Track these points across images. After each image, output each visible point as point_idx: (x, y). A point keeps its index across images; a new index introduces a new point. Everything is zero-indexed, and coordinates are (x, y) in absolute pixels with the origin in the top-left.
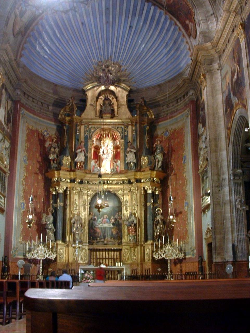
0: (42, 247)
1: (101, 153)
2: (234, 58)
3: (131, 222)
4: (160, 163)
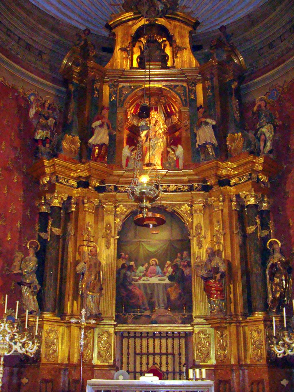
0: (7, 325)
3: (214, 268)
4: (269, 144)
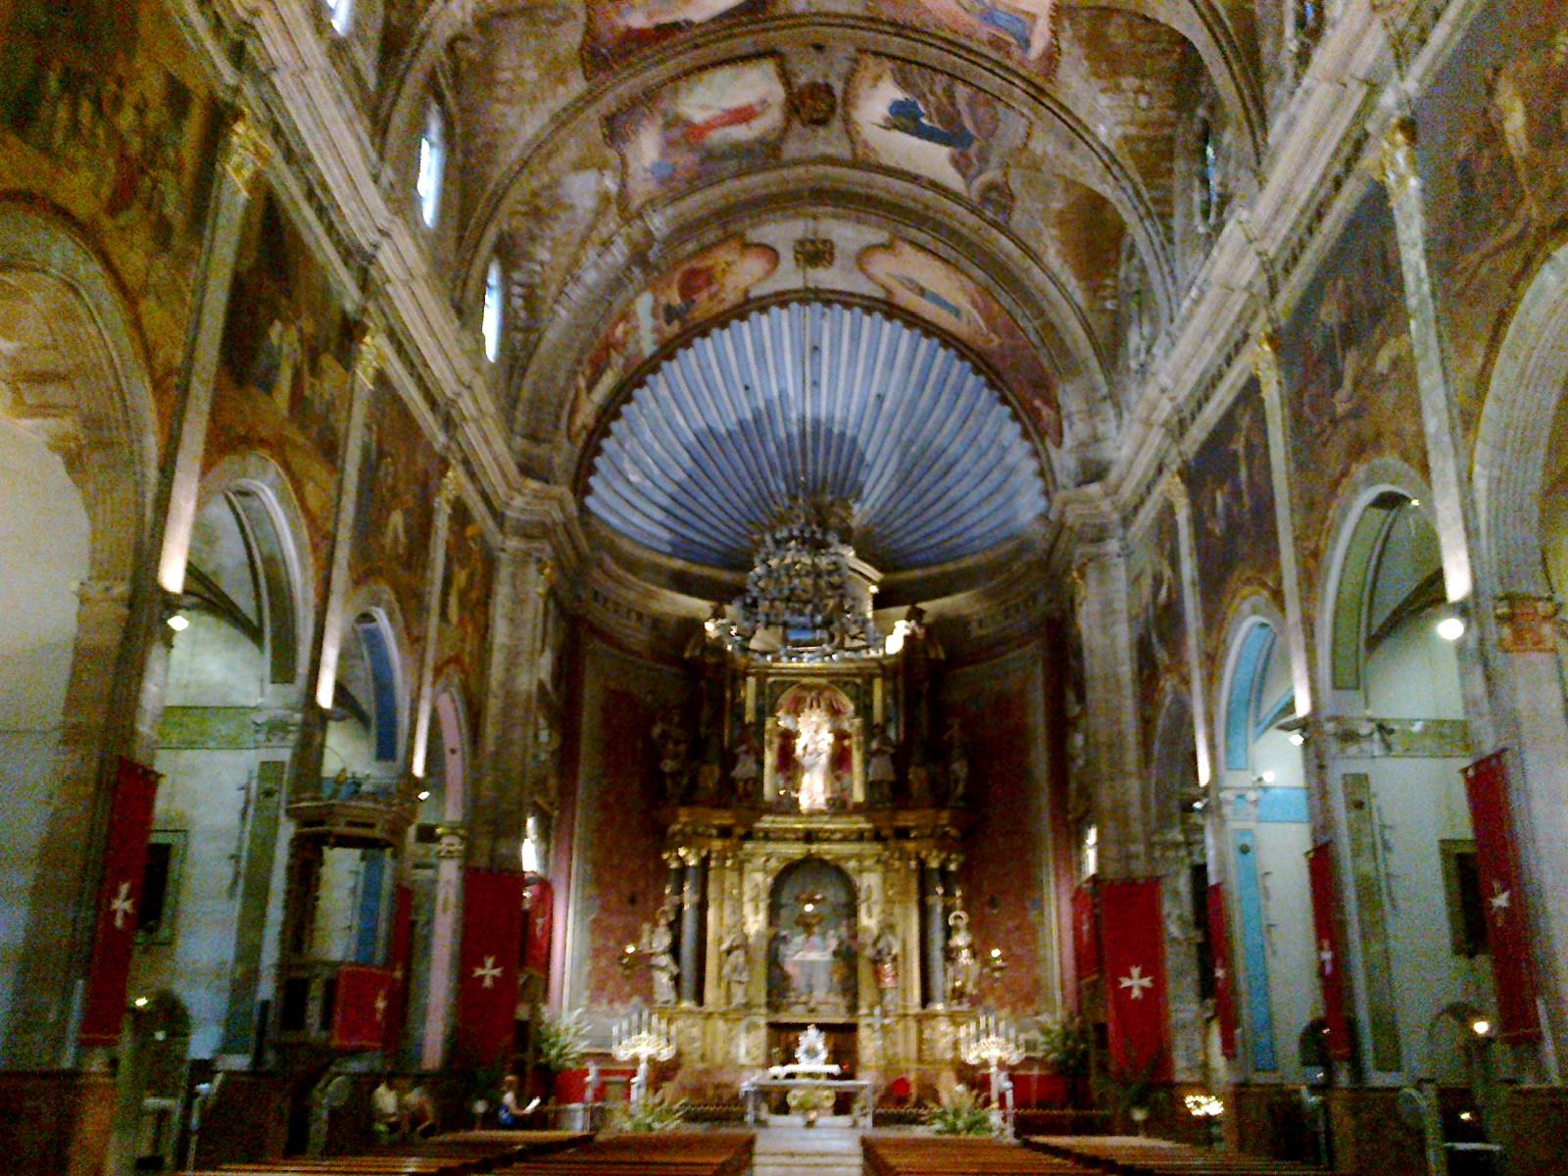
1: (799, 751)
2: (1162, 547)
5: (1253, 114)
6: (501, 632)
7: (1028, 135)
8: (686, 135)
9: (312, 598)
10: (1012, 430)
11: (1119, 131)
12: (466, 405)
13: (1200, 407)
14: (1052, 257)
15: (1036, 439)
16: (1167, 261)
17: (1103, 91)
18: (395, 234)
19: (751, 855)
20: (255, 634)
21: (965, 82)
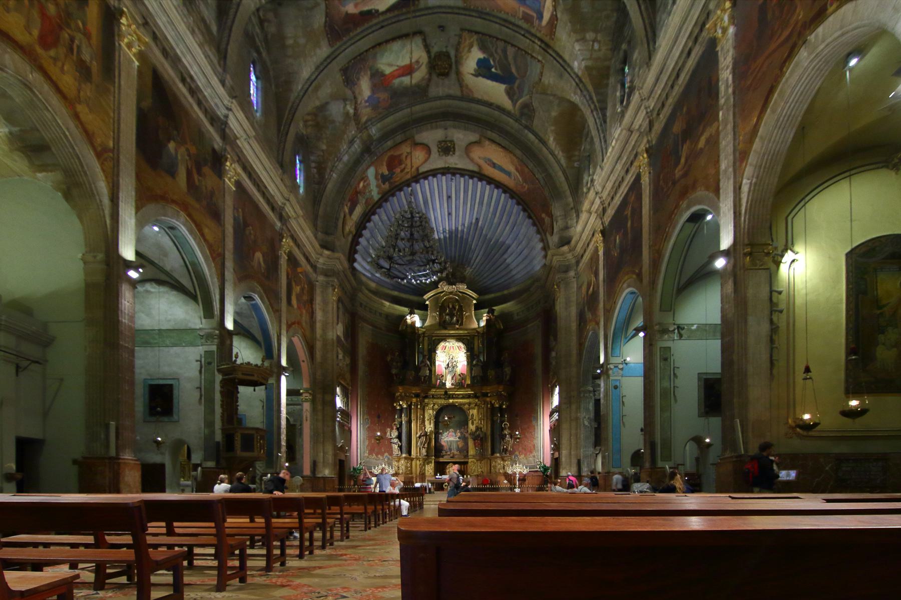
2: (592, 268)
5: (650, 34)
6: (319, 315)
7: (541, 73)
8: (380, 80)
9: (217, 284)
10: (533, 229)
11: (583, 64)
12: (288, 209)
13: (612, 198)
14: (551, 140)
15: (543, 234)
16: (603, 132)
17: (577, 41)
18: (234, 109)
19: (428, 404)
20: (194, 297)
21: (513, 45)
